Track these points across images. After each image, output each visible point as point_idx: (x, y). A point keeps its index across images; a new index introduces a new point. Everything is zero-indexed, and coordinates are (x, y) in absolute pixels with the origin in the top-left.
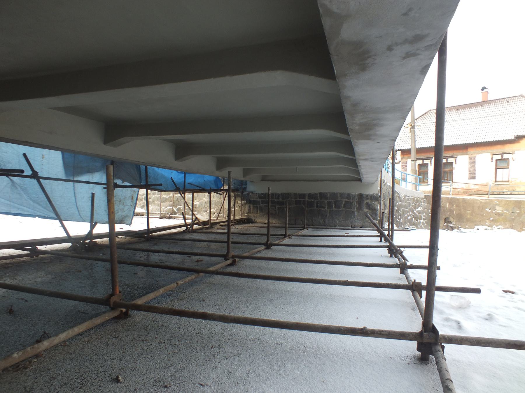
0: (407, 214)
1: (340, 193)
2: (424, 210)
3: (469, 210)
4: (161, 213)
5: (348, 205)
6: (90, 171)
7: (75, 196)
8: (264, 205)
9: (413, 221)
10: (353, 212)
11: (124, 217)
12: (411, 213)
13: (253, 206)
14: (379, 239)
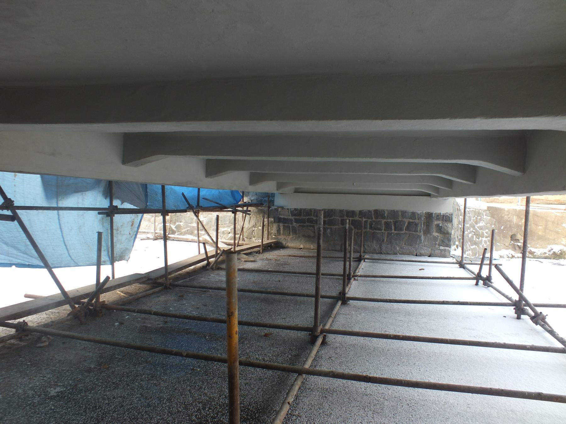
0: (468, 231)
1: (402, 211)
2: (487, 225)
3: (541, 226)
4: (156, 232)
5: (412, 226)
6: (79, 189)
7: (61, 228)
8: (298, 225)
9: (474, 239)
10: (419, 237)
11: (124, 250)
12: (472, 229)
13: (283, 226)
14: (474, 282)
